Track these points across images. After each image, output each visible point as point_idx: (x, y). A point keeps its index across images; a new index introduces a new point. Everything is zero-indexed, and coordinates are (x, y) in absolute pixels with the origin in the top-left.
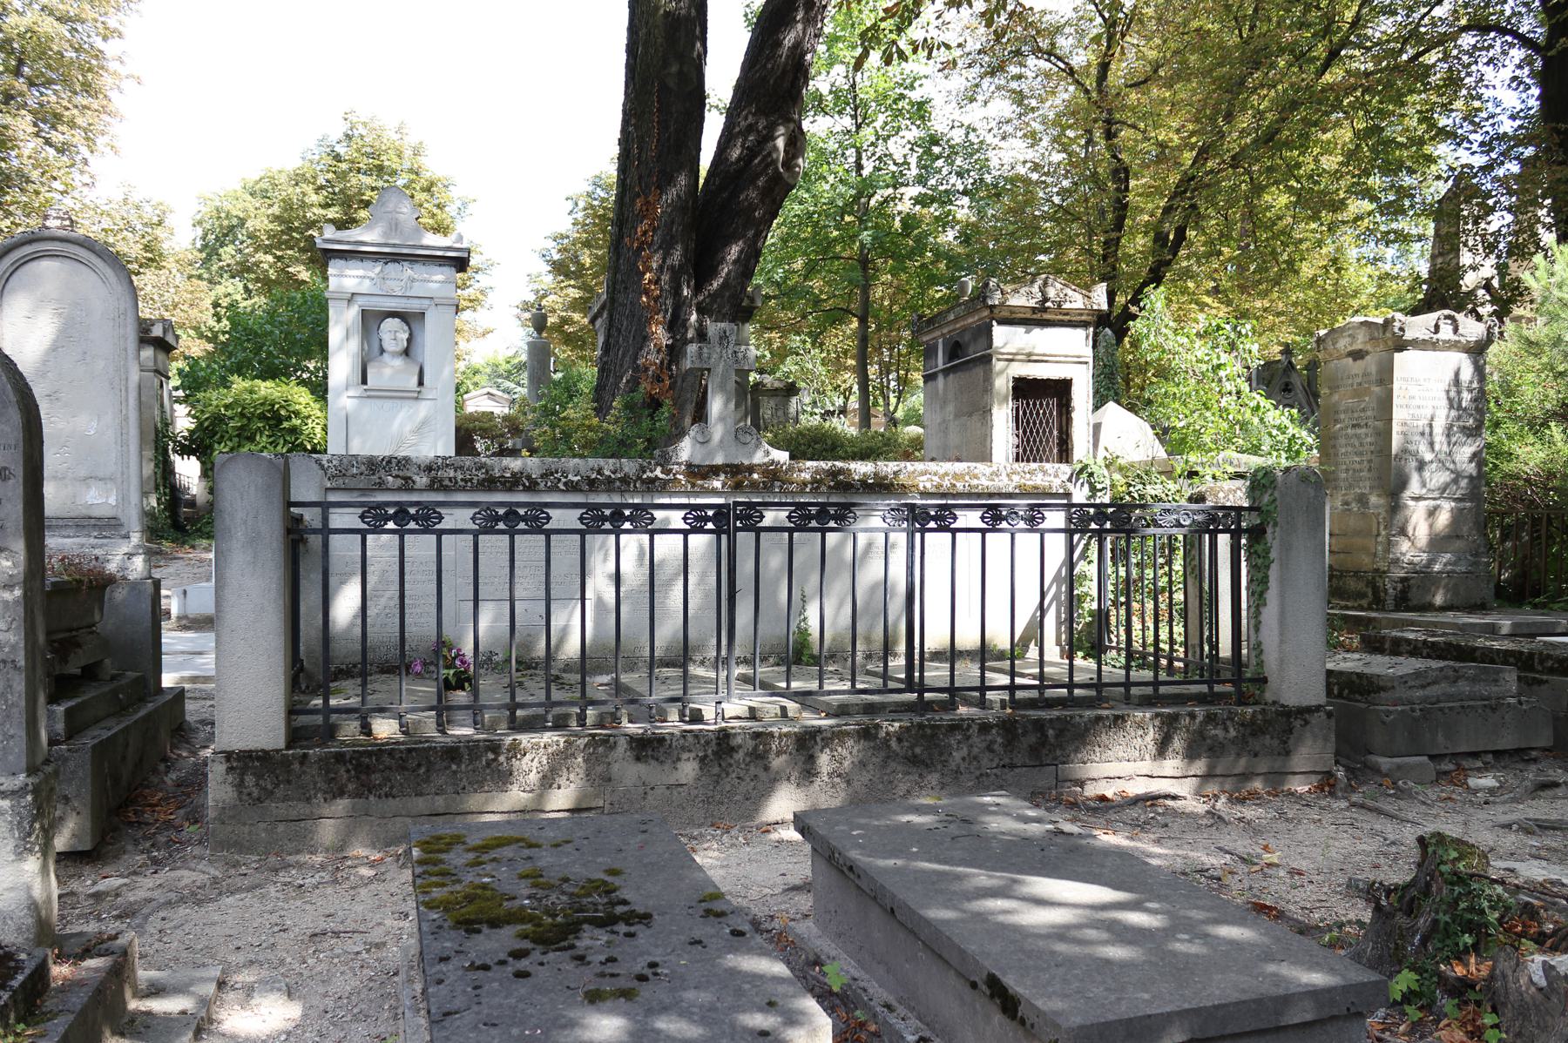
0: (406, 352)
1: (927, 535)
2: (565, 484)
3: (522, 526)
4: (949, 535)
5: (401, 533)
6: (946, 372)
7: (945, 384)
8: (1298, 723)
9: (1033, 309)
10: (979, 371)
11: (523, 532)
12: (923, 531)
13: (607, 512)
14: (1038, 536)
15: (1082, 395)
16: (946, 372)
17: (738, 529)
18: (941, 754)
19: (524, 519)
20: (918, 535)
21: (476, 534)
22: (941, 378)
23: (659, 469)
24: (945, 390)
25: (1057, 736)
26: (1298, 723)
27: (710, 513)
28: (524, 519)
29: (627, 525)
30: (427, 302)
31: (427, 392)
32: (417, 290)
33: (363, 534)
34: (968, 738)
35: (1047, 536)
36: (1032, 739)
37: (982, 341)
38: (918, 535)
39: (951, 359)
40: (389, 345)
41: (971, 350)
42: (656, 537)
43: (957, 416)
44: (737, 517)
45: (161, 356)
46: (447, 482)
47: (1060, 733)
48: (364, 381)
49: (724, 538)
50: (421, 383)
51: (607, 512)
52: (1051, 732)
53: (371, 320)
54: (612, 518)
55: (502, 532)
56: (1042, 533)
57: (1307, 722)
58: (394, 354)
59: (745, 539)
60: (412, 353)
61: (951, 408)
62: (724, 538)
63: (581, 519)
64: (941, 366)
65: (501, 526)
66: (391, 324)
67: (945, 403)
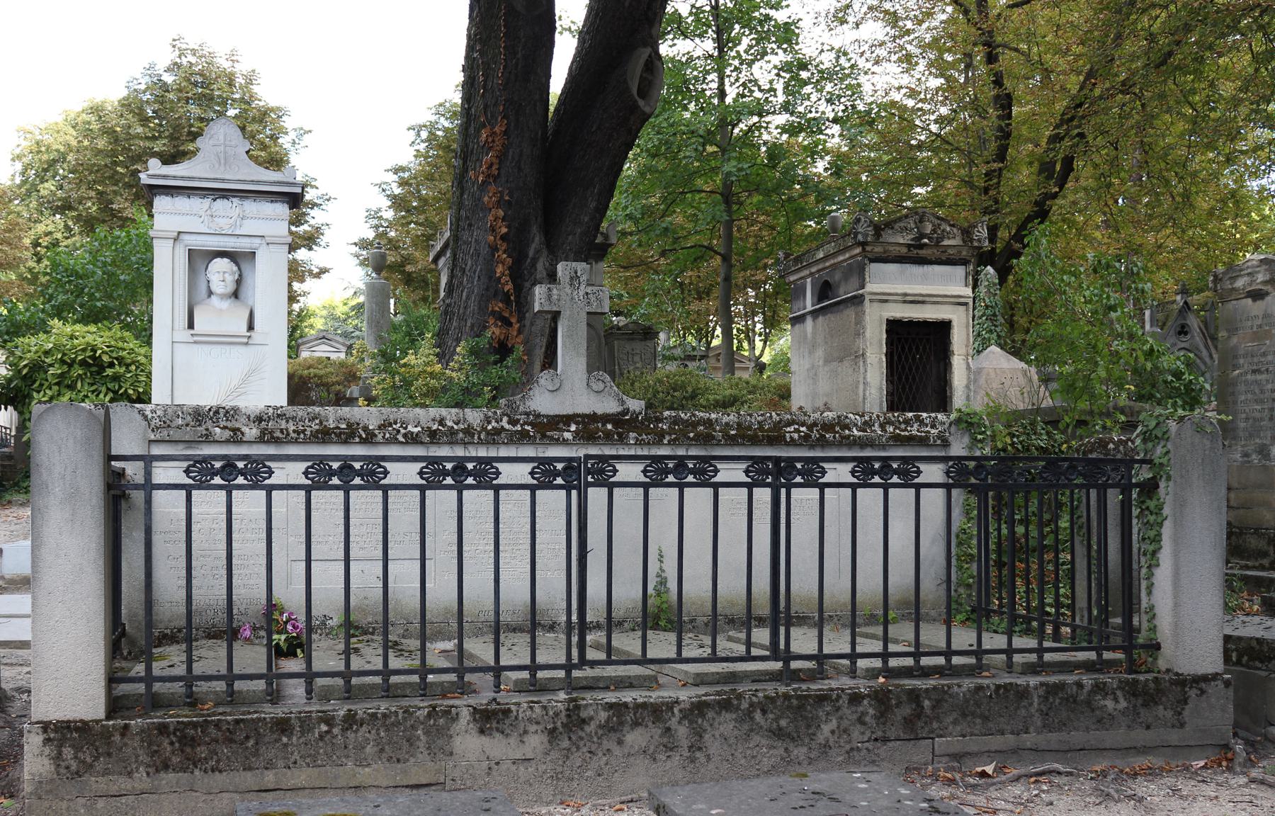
0: (236, 295)
1: (465, 493)
2: (405, 436)
6: (815, 314)
7: (814, 327)
8: (1193, 693)
9: (909, 246)
10: (850, 313)
11: (359, 487)
12: (789, 486)
15: (960, 339)
16: (815, 314)
17: (588, 485)
18: (808, 727)
20: (783, 491)
22: (809, 320)
23: (505, 419)
24: (814, 333)
25: (933, 708)
26: (1193, 693)
29: (470, 480)
30: (258, 241)
31: (257, 336)
32: (249, 227)
34: (838, 709)
36: (907, 710)
37: (854, 281)
38: (783, 491)
39: (820, 300)
40: (218, 287)
41: (841, 291)
42: (923, 491)
44: (588, 472)
46: (278, 434)
47: (937, 704)
48: (191, 326)
49: (574, 493)
50: (251, 327)
52: (927, 703)
53: (199, 259)
55: (336, 488)
57: (1203, 692)
58: (223, 297)
59: (597, 496)
60: (242, 295)
61: (820, 353)
62: (574, 493)
64: (809, 308)
66: (221, 264)
67: (814, 347)
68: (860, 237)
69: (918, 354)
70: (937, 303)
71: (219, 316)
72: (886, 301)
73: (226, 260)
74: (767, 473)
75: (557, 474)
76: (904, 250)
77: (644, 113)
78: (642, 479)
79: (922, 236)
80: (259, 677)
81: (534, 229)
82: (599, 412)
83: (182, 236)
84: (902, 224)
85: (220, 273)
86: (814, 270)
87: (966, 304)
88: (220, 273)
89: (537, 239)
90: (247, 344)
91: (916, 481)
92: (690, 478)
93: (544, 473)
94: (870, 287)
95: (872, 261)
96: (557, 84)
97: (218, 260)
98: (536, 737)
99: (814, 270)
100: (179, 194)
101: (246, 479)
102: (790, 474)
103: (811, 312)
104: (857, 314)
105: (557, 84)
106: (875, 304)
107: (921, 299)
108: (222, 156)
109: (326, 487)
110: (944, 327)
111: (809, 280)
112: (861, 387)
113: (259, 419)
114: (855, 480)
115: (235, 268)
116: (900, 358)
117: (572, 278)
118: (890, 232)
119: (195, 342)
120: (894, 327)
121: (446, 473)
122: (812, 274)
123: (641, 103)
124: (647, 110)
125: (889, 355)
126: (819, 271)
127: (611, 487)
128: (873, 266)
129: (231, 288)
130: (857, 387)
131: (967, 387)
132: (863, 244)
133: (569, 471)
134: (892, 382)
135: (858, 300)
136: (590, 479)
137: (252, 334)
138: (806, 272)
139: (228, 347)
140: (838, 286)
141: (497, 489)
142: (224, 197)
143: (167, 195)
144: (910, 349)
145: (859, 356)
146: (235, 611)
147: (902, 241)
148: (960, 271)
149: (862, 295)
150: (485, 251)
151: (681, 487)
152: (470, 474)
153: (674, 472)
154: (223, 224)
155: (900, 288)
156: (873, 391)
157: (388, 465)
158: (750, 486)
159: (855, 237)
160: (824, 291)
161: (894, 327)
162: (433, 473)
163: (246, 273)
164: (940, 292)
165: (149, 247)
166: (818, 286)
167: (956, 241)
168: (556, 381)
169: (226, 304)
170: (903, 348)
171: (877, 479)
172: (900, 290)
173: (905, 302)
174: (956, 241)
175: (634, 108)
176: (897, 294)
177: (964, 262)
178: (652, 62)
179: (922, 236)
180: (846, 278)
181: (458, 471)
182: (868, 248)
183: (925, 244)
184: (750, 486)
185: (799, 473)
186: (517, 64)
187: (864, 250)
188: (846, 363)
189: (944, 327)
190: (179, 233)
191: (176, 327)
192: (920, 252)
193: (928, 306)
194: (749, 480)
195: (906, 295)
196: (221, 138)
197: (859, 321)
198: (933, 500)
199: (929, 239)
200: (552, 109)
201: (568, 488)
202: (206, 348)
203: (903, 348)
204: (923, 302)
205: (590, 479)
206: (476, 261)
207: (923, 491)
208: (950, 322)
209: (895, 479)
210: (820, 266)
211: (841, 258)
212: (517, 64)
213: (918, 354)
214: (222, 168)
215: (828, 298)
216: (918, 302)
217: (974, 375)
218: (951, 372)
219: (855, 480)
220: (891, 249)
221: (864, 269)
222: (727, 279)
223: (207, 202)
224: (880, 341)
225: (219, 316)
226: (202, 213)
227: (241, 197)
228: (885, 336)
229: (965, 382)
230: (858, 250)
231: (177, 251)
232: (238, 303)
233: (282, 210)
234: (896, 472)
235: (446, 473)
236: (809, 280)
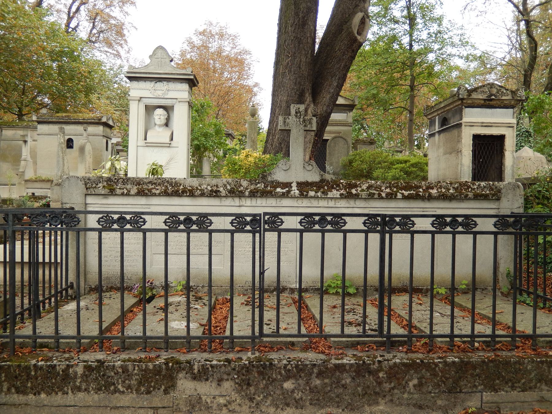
0: (167, 125)
1: (192, 234)
3: (128, 226)
4: (342, 235)
5: (454, 234)
6: (440, 132)
7: (439, 138)
9: (485, 100)
10: (455, 132)
11: (129, 230)
12: (391, 233)
13: (317, 218)
14: (342, 235)
15: (510, 144)
16: (440, 132)
17: (265, 230)
19: (461, 224)
20: (387, 236)
21: (301, 232)
22: (437, 136)
24: (439, 141)
27: (317, 218)
28: (129, 222)
29: (194, 227)
30: (175, 100)
31: (173, 143)
32: (171, 95)
33: (166, 232)
35: (148, 234)
37: (457, 117)
38: (387, 236)
39: (442, 126)
40: (158, 122)
41: (451, 121)
42: (478, 236)
43: (445, 154)
44: (266, 222)
45: (108, 130)
46: (146, 191)
48: (146, 139)
49: (257, 235)
50: (172, 139)
51: (248, 219)
53: (150, 109)
54: (319, 222)
55: (116, 230)
56: (144, 232)
58: (160, 126)
59: (271, 237)
60: (170, 125)
61: (441, 150)
62: (257, 235)
63: (364, 223)
64: (437, 130)
65: (115, 226)
66: (160, 111)
67: (439, 147)
68: (461, 96)
69: (489, 150)
70: (499, 126)
71: (158, 134)
72: (473, 126)
73: (161, 109)
74: (377, 224)
75: (247, 223)
76: (483, 102)
77: (360, 42)
78: (299, 227)
79: (492, 95)
80: (73, 338)
81: (307, 95)
82: (310, 181)
83: (143, 99)
84: (482, 90)
85: (159, 115)
86: (439, 112)
87: (513, 127)
88: (159, 115)
89: (308, 100)
90: (169, 147)
91: (474, 230)
92: (329, 227)
93: (239, 223)
94: (465, 120)
95: (466, 107)
96: (320, 32)
97: (158, 109)
98: (228, 382)
99: (439, 112)
100: (141, 80)
101: (131, 226)
102: (392, 225)
103: (438, 132)
104: (458, 132)
105: (320, 32)
106: (468, 127)
107: (490, 125)
108: (160, 63)
109: (110, 230)
110: (502, 138)
111: (437, 117)
112: (460, 166)
113: (138, 184)
114: (434, 229)
115: (166, 113)
116: (479, 152)
117: (296, 113)
118: (475, 93)
119: (147, 146)
120: (476, 138)
121: (180, 223)
122: (438, 115)
123: (359, 37)
124: (361, 41)
125: (474, 151)
126: (442, 113)
127: (280, 232)
128: (467, 109)
129: (164, 121)
130: (458, 166)
131: (513, 166)
132: (462, 99)
133: (254, 222)
134: (475, 164)
135: (459, 126)
136: (266, 227)
137: (172, 142)
138: (435, 114)
139: (161, 148)
140: (450, 120)
141: (211, 232)
142: (160, 81)
143: (136, 81)
144: (484, 148)
145: (459, 152)
146: (126, 278)
147: (481, 98)
148: (511, 111)
149: (461, 124)
150: (284, 105)
151: (323, 232)
152: (194, 223)
153: (319, 222)
154: (159, 93)
155: (480, 120)
156: (465, 168)
157: (146, 217)
158: (366, 232)
159: (458, 96)
160: (444, 121)
161: (476, 138)
162: (172, 222)
163: (171, 115)
164: (498, 121)
165: (127, 105)
166: (441, 120)
167: (510, 97)
168: (287, 165)
169: (161, 129)
170: (481, 148)
171: (448, 229)
172: (478, 121)
173: (482, 126)
174: (510, 97)
175: (356, 40)
176: (478, 123)
177: (513, 107)
178: (364, 19)
179: (492, 95)
180: (454, 116)
181: (187, 221)
182: (465, 101)
183: (493, 99)
184: (366, 232)
185: (398, 224)
186: (299, 20)
187: (462, 102)
188: (453, 155)
189: (502, 138)
190: (141, 98)
191: (139, 139)
192: (491, 103)
193: (494, 128)
194: (366, 228)
195: (483, 123)
196: (159, 55)
197: (459, 136)
198: (485, 244)
199: (495, 96)
200: (318, 41)
201: (253, 232)
202: (152, 149)
203: (481, 148)
204: (491, 126)
205: (266, 227)
206: (280, 110)
207: (478, 236)
208: (505, 135)
209: (460, 229)
210: (443, 111)
211: (452, 106)
212: (299, 20)
213: (489, 150)
214: (160, 68)
215: (446, 125)
216: (489, 126)
217: (516, 160)
218: (504, 159)
219: (434, 229)
220: (476, 101)
221: (462, 111)
222: (411, 120)
223: (153, 83)
224: (469, 145)
225: (158, 134)
226: (150, 88)
227: (168, 81)
228: (472, 142)
229: (511, 164)
230: (460, 102)
231: (140, 106)
232: (167, 128)
233: (186, 86)
234: (461, 224)
235: (180, 223)
236: (437, 117)
